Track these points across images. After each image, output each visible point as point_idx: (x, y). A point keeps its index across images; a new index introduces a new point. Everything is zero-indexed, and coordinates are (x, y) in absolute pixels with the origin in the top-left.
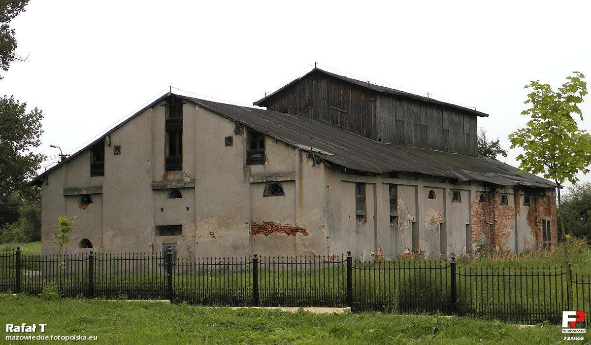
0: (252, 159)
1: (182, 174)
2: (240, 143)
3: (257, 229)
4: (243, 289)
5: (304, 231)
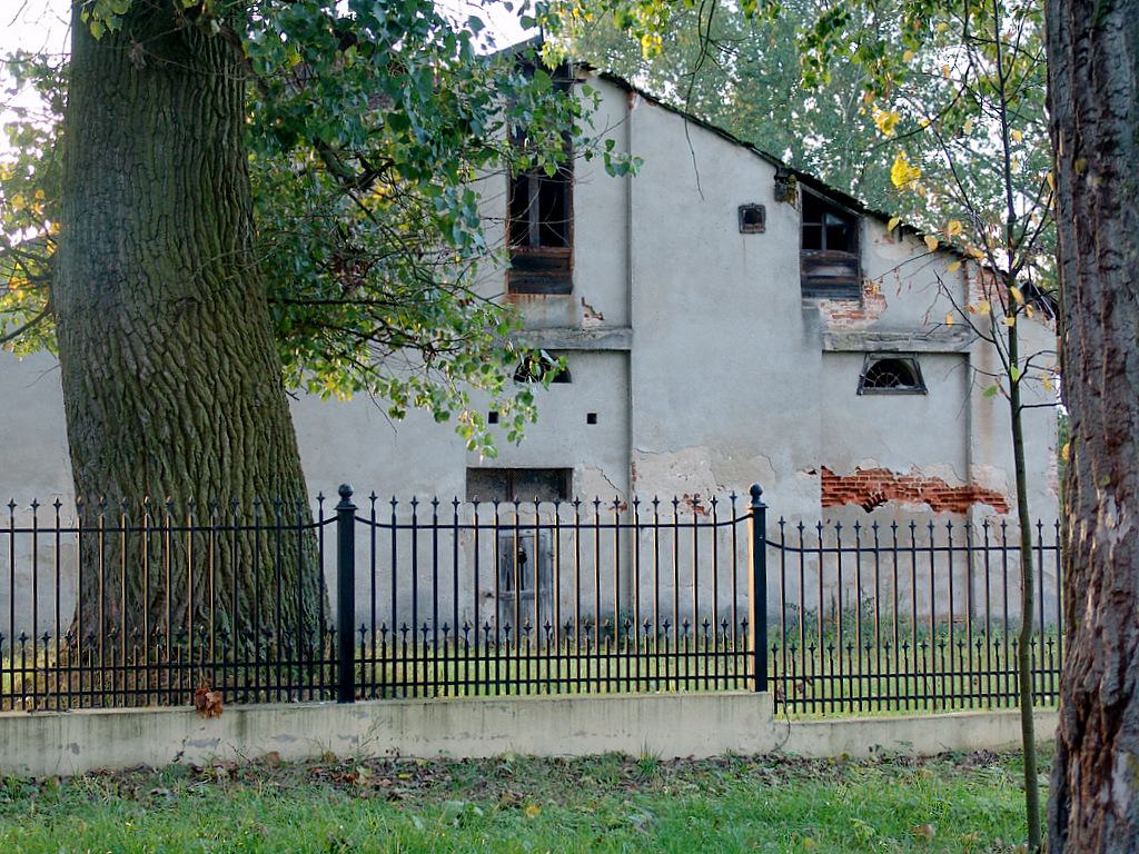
1: (572, 308)
2: (785, 224)
4: (405, 630)
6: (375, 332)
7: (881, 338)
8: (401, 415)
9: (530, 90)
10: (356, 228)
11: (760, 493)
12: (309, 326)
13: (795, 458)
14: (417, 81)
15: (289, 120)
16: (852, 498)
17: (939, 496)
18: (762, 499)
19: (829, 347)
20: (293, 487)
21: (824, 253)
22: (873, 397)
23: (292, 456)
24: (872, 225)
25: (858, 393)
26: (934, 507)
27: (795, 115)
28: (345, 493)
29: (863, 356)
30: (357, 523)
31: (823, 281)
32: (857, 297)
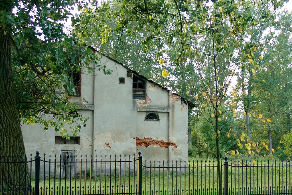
0: (137, 95)
1: (81, 100)
2: (129, 82)
3: (140, 142)
5: (174, 145)
6: (42, 109)
7: (150, 108)
8: (47, 129)
9: (86, 53)
10: (38, 84)
11: (141, 154)
12: (25, 108)
13: (131, 135)
14: (59, 50)
15: (23, 57)
16: (143, 144)
17: (162, 144)
18: (141, 155)
19: (138, 110)
20: (22, 149)
21: (138, 89)
22: (148, 121)
23: (22, 141)
24: (149, 83)
25: (145, 121)
26: (161, 146)
27: (125, 56)
28: (38, 153)
29: (146, 112)
30: (40, 161)
31: (138, 95)
32: (145, 99)
